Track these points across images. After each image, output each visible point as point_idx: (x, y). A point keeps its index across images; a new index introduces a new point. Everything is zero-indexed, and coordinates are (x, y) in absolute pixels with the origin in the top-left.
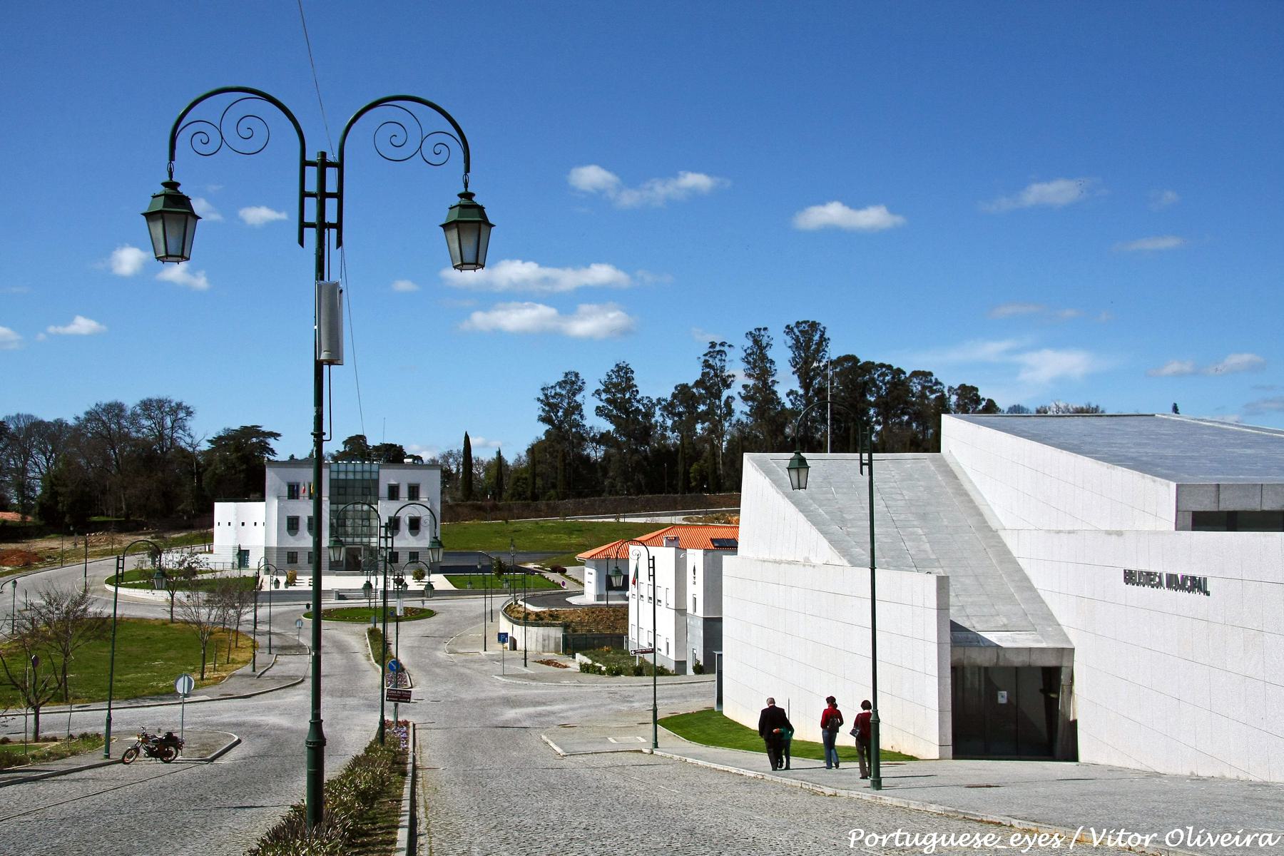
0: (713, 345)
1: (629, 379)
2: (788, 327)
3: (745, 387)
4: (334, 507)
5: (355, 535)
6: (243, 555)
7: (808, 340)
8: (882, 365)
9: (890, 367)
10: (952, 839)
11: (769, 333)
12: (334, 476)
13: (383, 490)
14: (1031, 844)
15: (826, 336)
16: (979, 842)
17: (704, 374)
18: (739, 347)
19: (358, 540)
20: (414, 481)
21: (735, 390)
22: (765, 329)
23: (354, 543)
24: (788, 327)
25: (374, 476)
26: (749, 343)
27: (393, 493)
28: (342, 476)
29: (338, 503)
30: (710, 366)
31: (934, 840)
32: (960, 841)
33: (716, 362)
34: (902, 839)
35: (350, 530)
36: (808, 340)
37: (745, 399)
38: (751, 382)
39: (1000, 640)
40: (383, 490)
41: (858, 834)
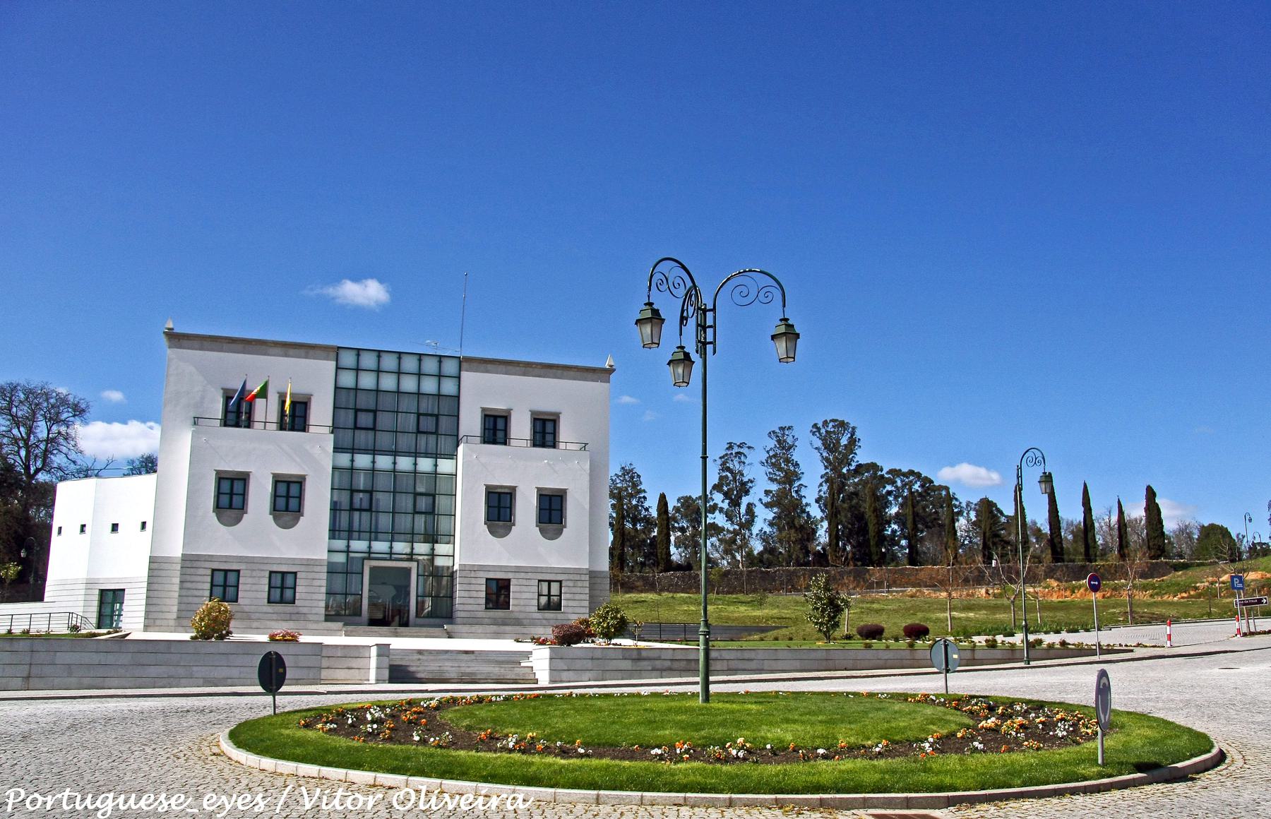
0: (730, 446)
1: (635, 485)
2: (815, 426)
3: (767, 492)
4: (344, 460)
5: (393, 536)
6: (110, 600)
7: (837, 443)
8: (911, 472)
9: (918, 475)
10: (132, 801)
11: (796, 433)
12: (347, 380)
13: (470, 422)
14: (228, 807)
15: (858, 435)
16: (165, 804)
17: (721, 478)
18: (762, 446)
19: (401, 547)
20: (546, 406)
21: (755, 496)
22: (789, 428)
23: (391, 555)
24: (815, 426)
25: (448, 387)
26: (772, 443)
27: (495, 428)
28: (367, 381)
29: (353, 450)
30: (728, 469)
31: (109, 802)
32: (142, 803)
33: (735, 465)
34: (71, 800)
35: (385, 521)
36: (837, 443)
37: (767, 505)
38: (774, 487)
39: (1063, 688)
40: (470, 422)
41: (17, 795)
